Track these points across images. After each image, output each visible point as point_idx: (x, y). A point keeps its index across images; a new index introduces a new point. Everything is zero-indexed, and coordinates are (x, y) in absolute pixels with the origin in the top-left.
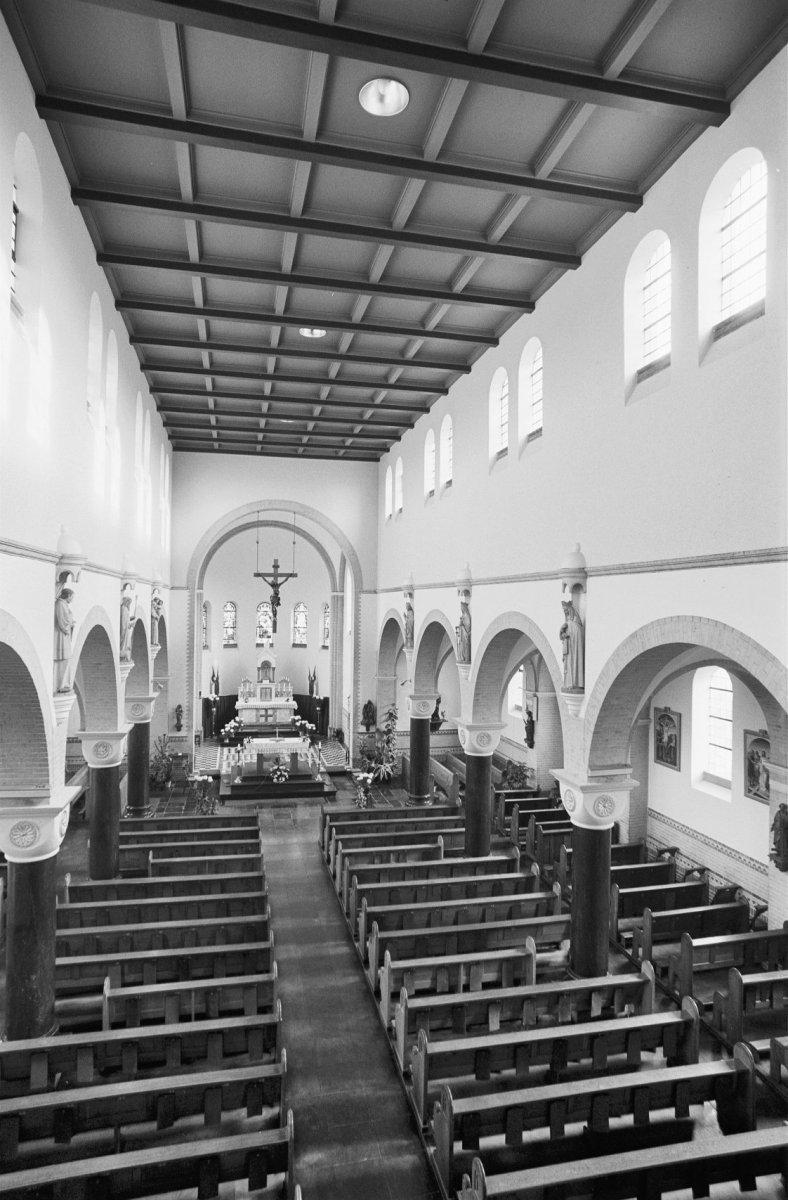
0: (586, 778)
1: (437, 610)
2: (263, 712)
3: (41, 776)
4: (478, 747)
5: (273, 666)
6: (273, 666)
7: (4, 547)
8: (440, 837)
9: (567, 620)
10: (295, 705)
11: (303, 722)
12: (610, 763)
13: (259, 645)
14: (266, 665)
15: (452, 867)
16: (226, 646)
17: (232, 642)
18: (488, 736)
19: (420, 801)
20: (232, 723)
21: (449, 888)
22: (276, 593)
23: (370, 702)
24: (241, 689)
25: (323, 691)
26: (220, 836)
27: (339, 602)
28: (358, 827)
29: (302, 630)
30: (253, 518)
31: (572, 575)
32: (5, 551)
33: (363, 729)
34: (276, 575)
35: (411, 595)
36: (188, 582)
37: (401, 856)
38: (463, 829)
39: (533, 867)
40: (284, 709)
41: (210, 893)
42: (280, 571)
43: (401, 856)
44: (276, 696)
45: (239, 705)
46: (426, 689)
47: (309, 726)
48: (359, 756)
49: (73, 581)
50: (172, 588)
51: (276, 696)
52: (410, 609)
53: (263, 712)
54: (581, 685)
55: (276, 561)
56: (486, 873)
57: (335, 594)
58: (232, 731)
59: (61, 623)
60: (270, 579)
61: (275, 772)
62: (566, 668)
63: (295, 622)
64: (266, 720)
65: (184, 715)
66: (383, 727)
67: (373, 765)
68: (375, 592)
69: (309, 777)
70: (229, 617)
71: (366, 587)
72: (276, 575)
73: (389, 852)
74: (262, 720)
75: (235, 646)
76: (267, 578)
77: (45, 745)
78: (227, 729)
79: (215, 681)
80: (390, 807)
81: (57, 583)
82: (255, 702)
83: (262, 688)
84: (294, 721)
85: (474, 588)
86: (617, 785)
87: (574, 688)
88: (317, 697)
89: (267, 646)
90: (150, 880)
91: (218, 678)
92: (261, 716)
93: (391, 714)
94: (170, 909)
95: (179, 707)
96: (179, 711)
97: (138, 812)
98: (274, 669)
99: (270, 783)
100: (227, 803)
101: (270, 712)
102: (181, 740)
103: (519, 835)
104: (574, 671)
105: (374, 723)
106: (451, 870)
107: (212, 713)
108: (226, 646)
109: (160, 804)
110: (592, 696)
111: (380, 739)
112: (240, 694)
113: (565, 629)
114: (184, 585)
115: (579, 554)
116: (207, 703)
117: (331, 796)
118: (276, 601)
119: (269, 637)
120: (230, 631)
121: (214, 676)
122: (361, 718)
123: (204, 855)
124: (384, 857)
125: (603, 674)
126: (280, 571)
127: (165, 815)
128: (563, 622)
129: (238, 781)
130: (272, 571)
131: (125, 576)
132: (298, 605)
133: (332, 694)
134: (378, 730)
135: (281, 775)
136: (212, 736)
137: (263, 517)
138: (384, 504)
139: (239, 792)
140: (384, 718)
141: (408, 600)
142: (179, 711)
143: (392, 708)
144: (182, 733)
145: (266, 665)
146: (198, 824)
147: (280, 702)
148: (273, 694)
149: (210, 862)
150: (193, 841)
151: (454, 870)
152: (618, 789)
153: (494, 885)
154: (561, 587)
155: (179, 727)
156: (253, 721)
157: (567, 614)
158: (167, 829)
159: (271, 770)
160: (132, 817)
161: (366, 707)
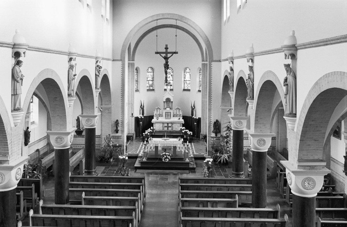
0: (297, 167)
1: (270, 71)
2: (166, 125)
3: (5, 150)
4: (258, 146)
5: (172, 101)
6: (172, 101)
7: (2, 45)
8: (237, 195)
9: (287, 75)
10: (182, 121)
11: (186, 130)
12: (311, 158)
13: (165, 90)
14: (168, 100)
15: (241, 212)
16: (148, 90)
17: (151, 88)
18: (264, 141)
19: (238, 175)
20: (149, 130)
21: (265, 225)
22: (167, 62)
23: (217, 121)
24: (155, 113)
25: (198, 114)
26: (123, 187)
27: (206, 67)
28: (196, 187)
29: (188, 82)
30: (154, 25)
31: (289, 49)
32: (2, 46)
33: (213, 135)
34: (167, 53)
35: (233, 63)
36: (121, 57)
37: (214, 204)
38: (251, 192)
39: (285, 216)
40: (178, 126)
41: (109, 215)
42: (169, 51)
43: (214, 204)
44: (174, 116)
45: (153, 121)
46: (241, 114)
47: (189, 132)
48: (211, 149)
49: (73, 60)
50: (113, 60)
51: (174, 116)
52: (232, 70)
53: (166, 125)
54: (294, 112)
55: (167, 45)
56: (261, 217)
57: (203, 62)
58: (149, 134)
59: (15, 76)
60: (164, 55)
61: (163, 156)
62: (286, 103)
63: (185, 78)
64: (168, 129)
65: (120, 125)
66: (224, 134)
67: (218, 154)
68: (220, 61)
69: (182, 159)
70: (150, 75)
71: (215, 58)
72: (167, 53)
73: (208, 201)
74: (166, 129)
75: (153, 90)
76: (162, 55)
77: (6, 136)
78: (146, 133)
79: (142, 108)
80: (223, 178)
81: (68, 61)
82: (162, 119)
83: (166, 112)
84: (181, 130)
85: (255, 57)
86: (316, 171)
87: (290, 114)
88: (195, 118)
89: (168, 90)
90: (83, 206)
91: (143, 107)
92: (165, 127)
93: (228, 127)
94: (100, 222)
95: (117, 121)
96: (117, 123)
97: (89, 173)
98: (172, 102)
99: (160, 161)
100: (138, 171)
101: (170, 125)
102: (118, 137)
103: (290, 198)
104: (291, 105)
105: (220, 132)
106: (240, 214)
107: (140, 124)
108: (148, 90)
109: (104, 170)
110: (299, 118)
111: (222, 141)
112: (155, 115)
113: (286, 80)
114: (119, 58)
115: (294, 37)
116: (137, 120)
117: (193, 170)
118: (167, 66)
119: (171, 86)
120: (151, 82)
121: (141, 105)
122: (212, 129)
123: (113, 196)
124: (205, 204)
125: (304, 106)
126: (169, 51)
127: (105, 175)
128: (286, 76)
129: (144, 160)
130: (164, 51)
131: (70, 54)
132: (186, 69)
133: (202, 116)
134: (221, 136)
135: (166, 158)
136: (140, 136)
137: (160, 23)
138: (223, 17)
139: (145, 166)
140: (225, 129)
141: (231, 65)
142: (117, 123)
143: (228, 124)
144: (119, 134)
145: (168, 100)
146: (115, 180)
147: (176, 119)
148: (172, 116)
149: (112, 199)
150: (110, 188)
151: (242, 214)
152: (317, 174)
153: (262, 225)
154: (284, 56)
155: (117, 131)
156: (161, 129)
157: (287, 71)
158: (99, 182)
159: (162, 155)
160: (87, 175)
161: (215, 123)
